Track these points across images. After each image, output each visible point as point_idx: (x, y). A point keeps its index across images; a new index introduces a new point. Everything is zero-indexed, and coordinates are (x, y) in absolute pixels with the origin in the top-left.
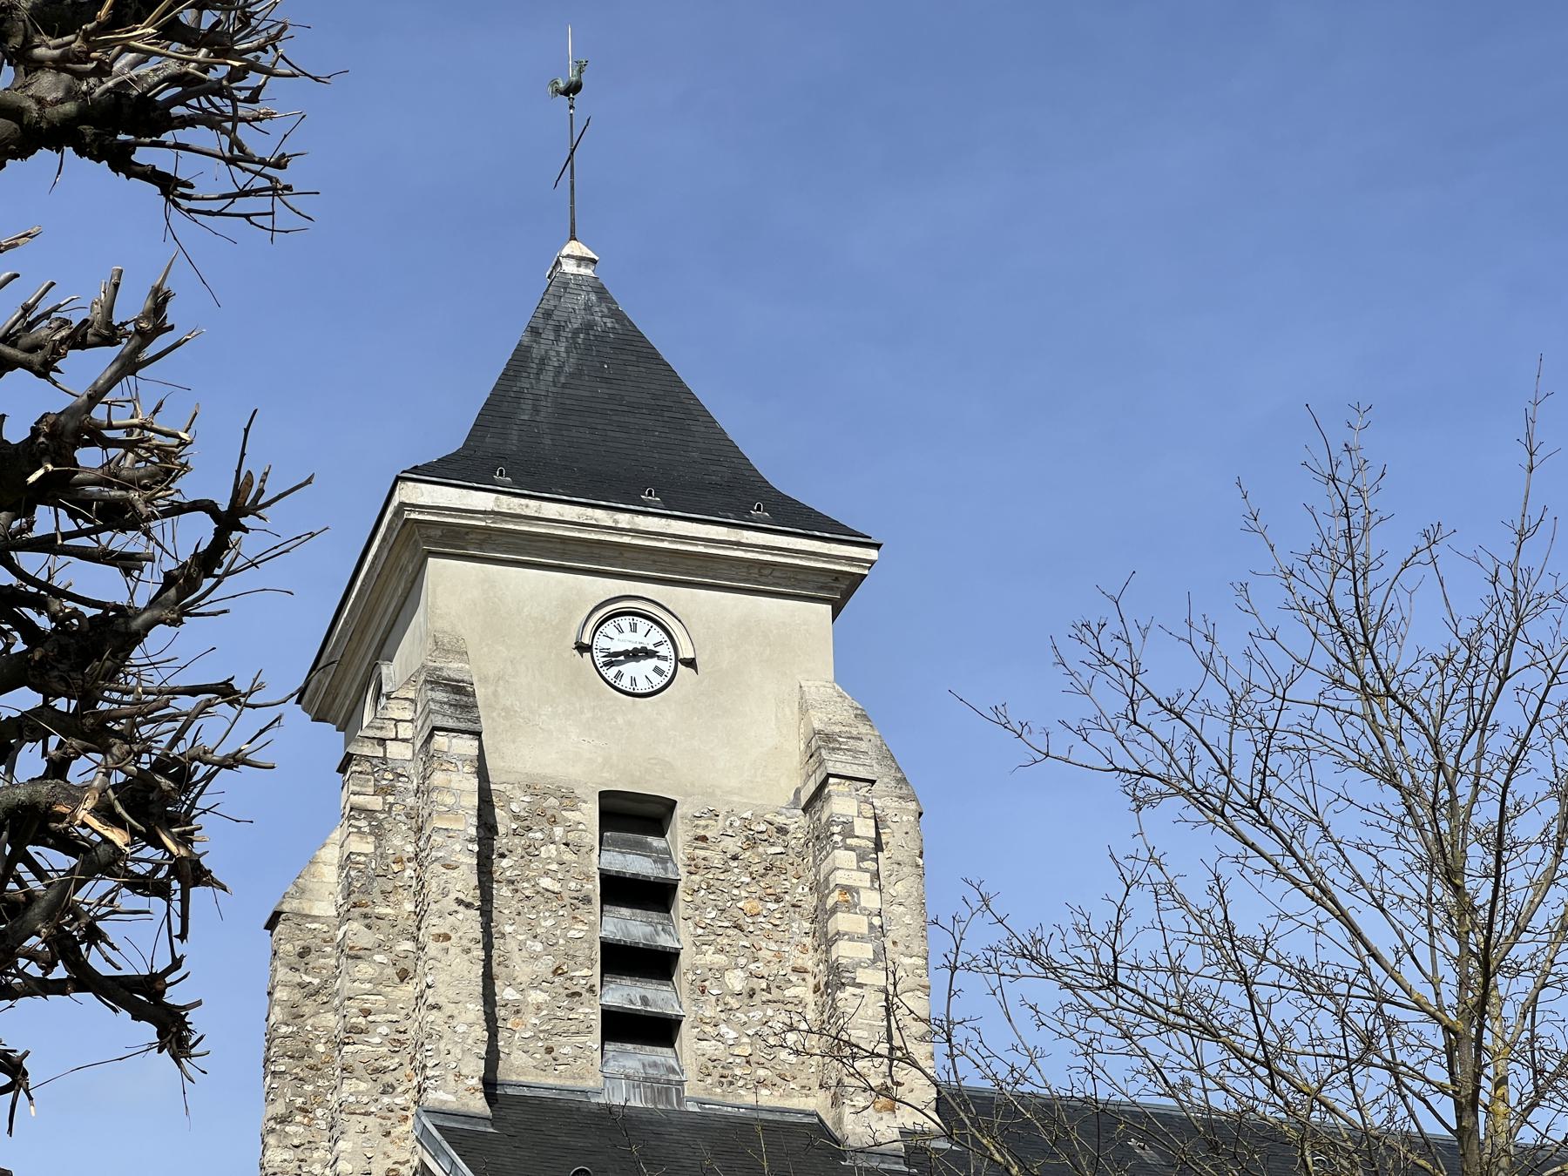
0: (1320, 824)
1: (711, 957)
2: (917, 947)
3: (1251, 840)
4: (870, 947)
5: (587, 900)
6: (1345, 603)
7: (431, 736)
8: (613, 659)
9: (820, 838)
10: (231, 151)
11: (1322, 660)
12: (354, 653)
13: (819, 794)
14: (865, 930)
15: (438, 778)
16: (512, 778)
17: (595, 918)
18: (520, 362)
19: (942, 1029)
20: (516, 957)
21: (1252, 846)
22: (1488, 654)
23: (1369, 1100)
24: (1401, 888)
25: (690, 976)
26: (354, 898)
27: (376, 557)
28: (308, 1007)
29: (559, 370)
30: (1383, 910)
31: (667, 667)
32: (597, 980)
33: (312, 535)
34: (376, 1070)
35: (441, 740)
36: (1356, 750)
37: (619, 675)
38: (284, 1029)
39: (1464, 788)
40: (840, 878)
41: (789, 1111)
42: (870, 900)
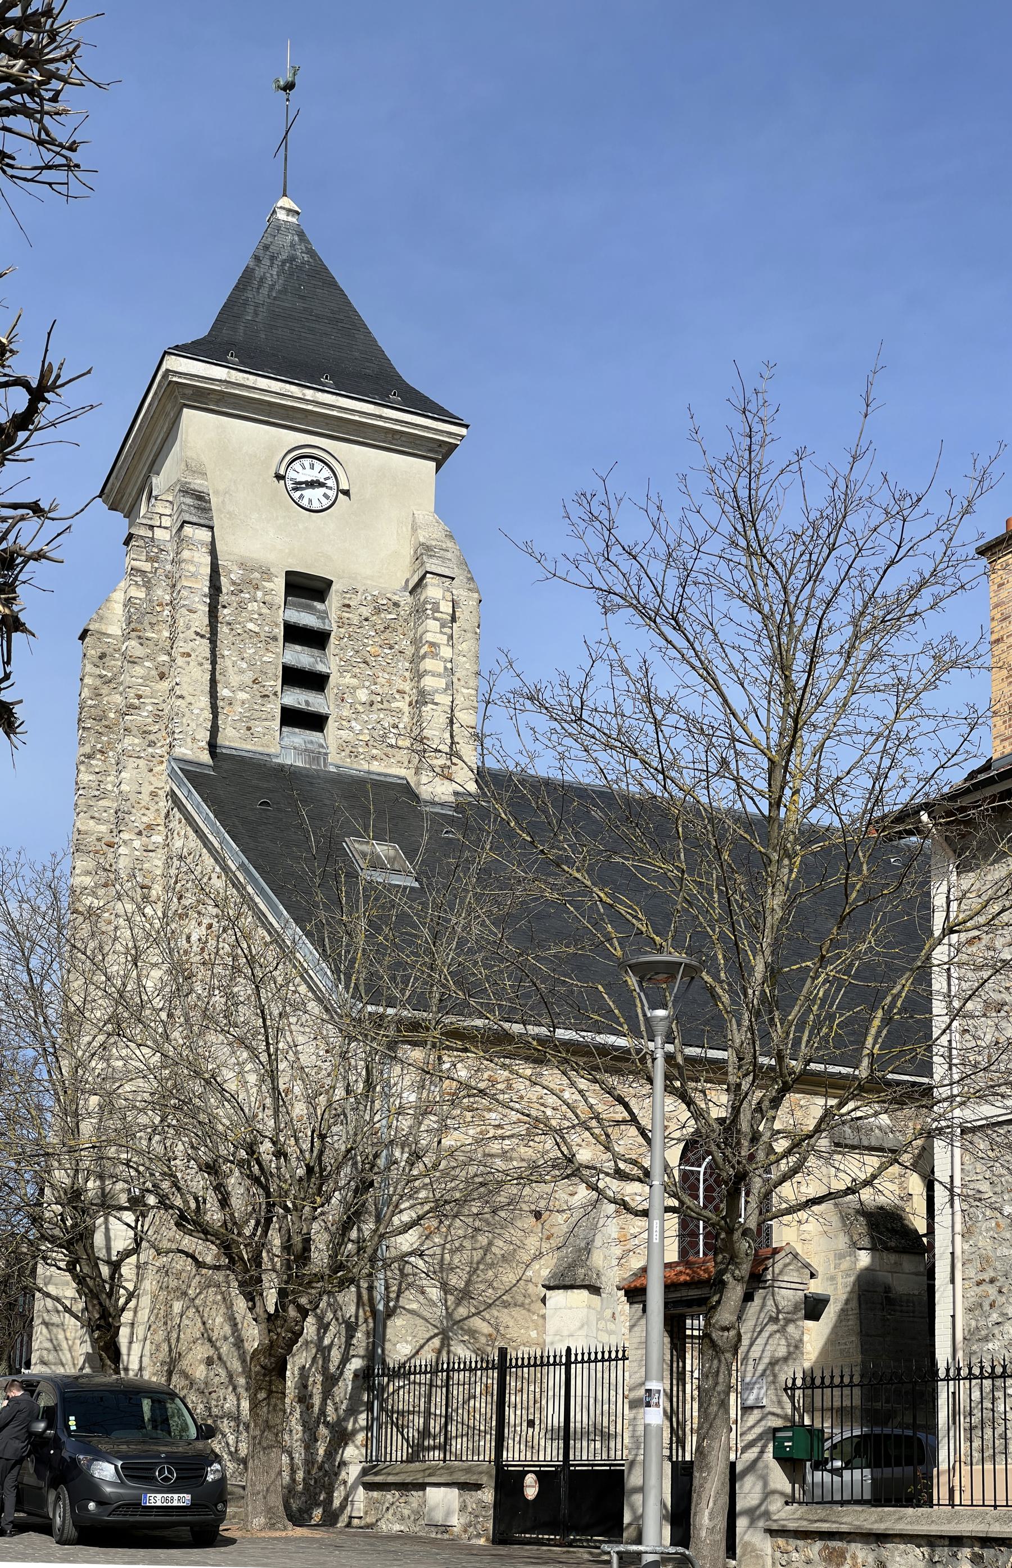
0: (713, 631)
1: (348, 680)
2: (472, 683)
3: (670, 638)
4: (444, 681)
5: (275, 639)
6: (742, 493)
7: (182, 526)
8: (298, 486)
9: (419, 611)
10: (39, 135)
11: (726, 528)
12: (135, 468)
13: (420, 583)
14: (442, 670)
15: (186, 554)
16: (232, 558)
17: (280, 650)
18: (247, 275)
19: (479, 738)
20: (231, 671)
21: (670, 642)
22: (824, 533)
23: (722, 793)
24: (755, 673)
25: (335, 691)
26: (133, 626)
27: (150, 405)
28: (105, 690)
29: (272, 287)
30: (742, 684)
31: (332, 494)
32: (279, 688)
33: (92, 407)
34: (145, 732)
35: (188, 530)
36: (738, 588)
37: (301, 497)
38: (90, 702)
39: (799, 616)
40: (429, 637)
41: (390, 775)
42: (446, 652)
